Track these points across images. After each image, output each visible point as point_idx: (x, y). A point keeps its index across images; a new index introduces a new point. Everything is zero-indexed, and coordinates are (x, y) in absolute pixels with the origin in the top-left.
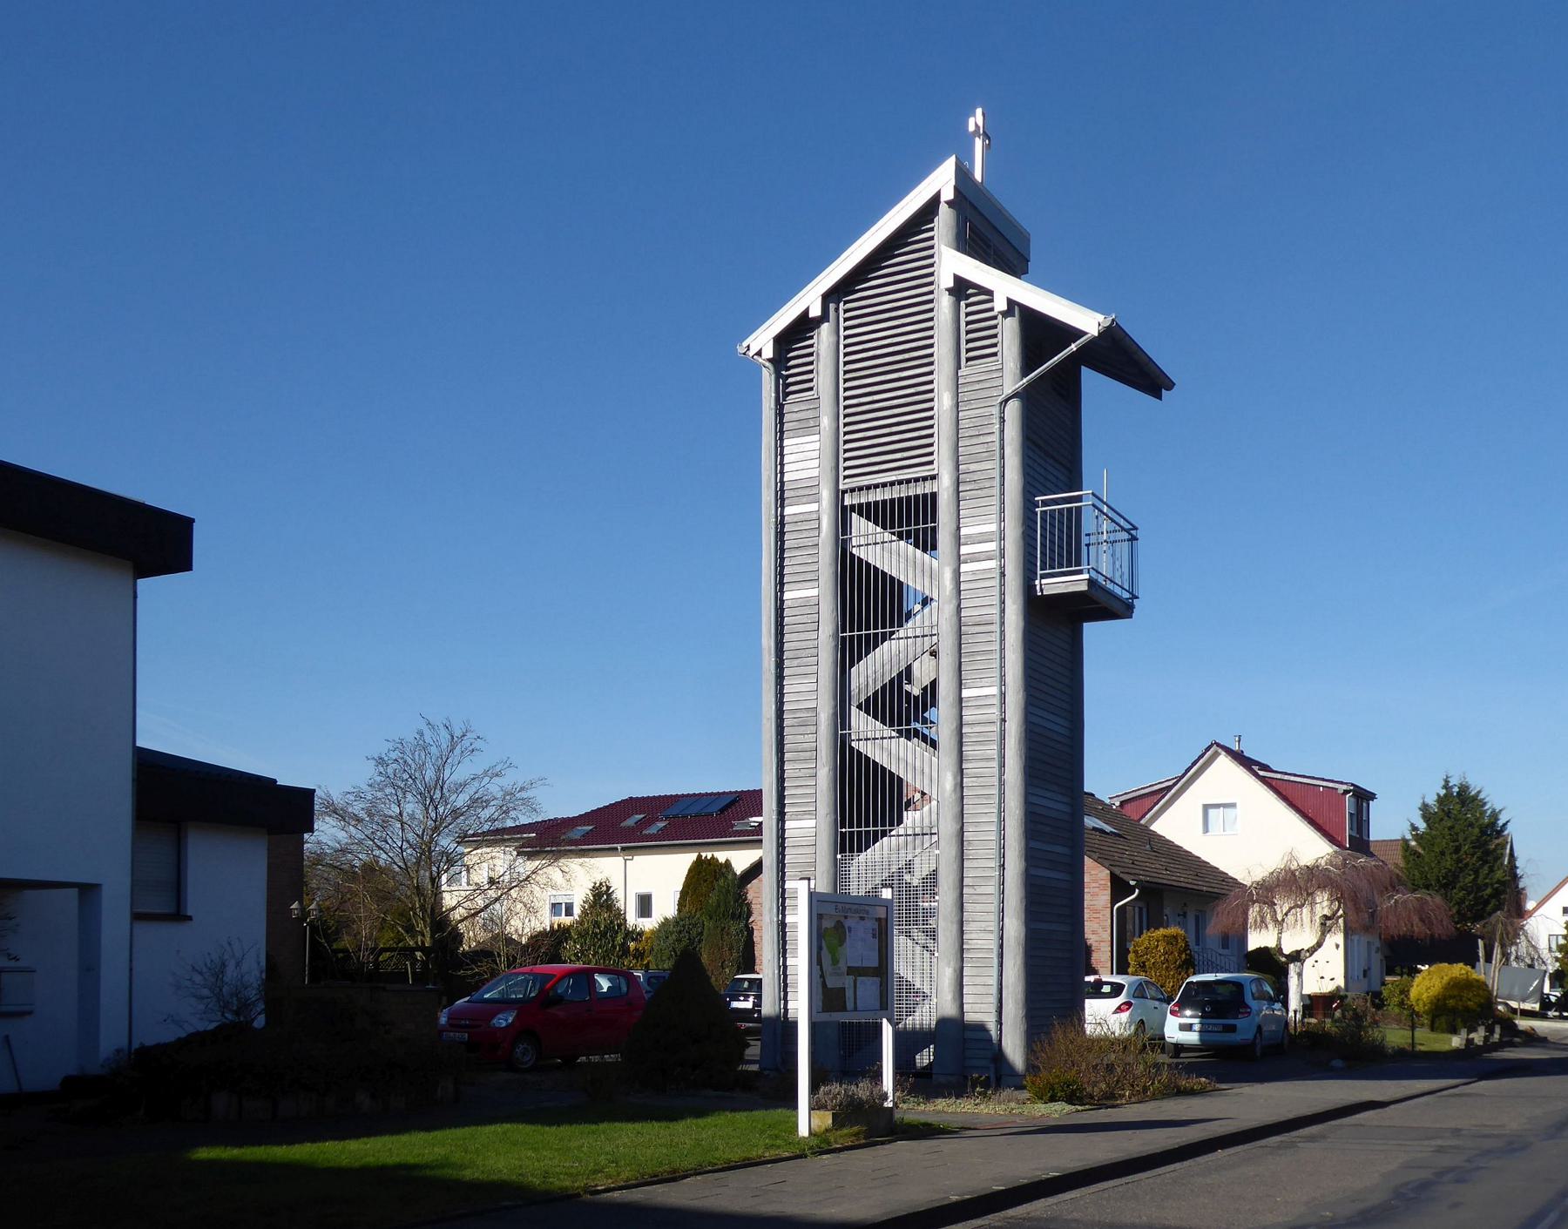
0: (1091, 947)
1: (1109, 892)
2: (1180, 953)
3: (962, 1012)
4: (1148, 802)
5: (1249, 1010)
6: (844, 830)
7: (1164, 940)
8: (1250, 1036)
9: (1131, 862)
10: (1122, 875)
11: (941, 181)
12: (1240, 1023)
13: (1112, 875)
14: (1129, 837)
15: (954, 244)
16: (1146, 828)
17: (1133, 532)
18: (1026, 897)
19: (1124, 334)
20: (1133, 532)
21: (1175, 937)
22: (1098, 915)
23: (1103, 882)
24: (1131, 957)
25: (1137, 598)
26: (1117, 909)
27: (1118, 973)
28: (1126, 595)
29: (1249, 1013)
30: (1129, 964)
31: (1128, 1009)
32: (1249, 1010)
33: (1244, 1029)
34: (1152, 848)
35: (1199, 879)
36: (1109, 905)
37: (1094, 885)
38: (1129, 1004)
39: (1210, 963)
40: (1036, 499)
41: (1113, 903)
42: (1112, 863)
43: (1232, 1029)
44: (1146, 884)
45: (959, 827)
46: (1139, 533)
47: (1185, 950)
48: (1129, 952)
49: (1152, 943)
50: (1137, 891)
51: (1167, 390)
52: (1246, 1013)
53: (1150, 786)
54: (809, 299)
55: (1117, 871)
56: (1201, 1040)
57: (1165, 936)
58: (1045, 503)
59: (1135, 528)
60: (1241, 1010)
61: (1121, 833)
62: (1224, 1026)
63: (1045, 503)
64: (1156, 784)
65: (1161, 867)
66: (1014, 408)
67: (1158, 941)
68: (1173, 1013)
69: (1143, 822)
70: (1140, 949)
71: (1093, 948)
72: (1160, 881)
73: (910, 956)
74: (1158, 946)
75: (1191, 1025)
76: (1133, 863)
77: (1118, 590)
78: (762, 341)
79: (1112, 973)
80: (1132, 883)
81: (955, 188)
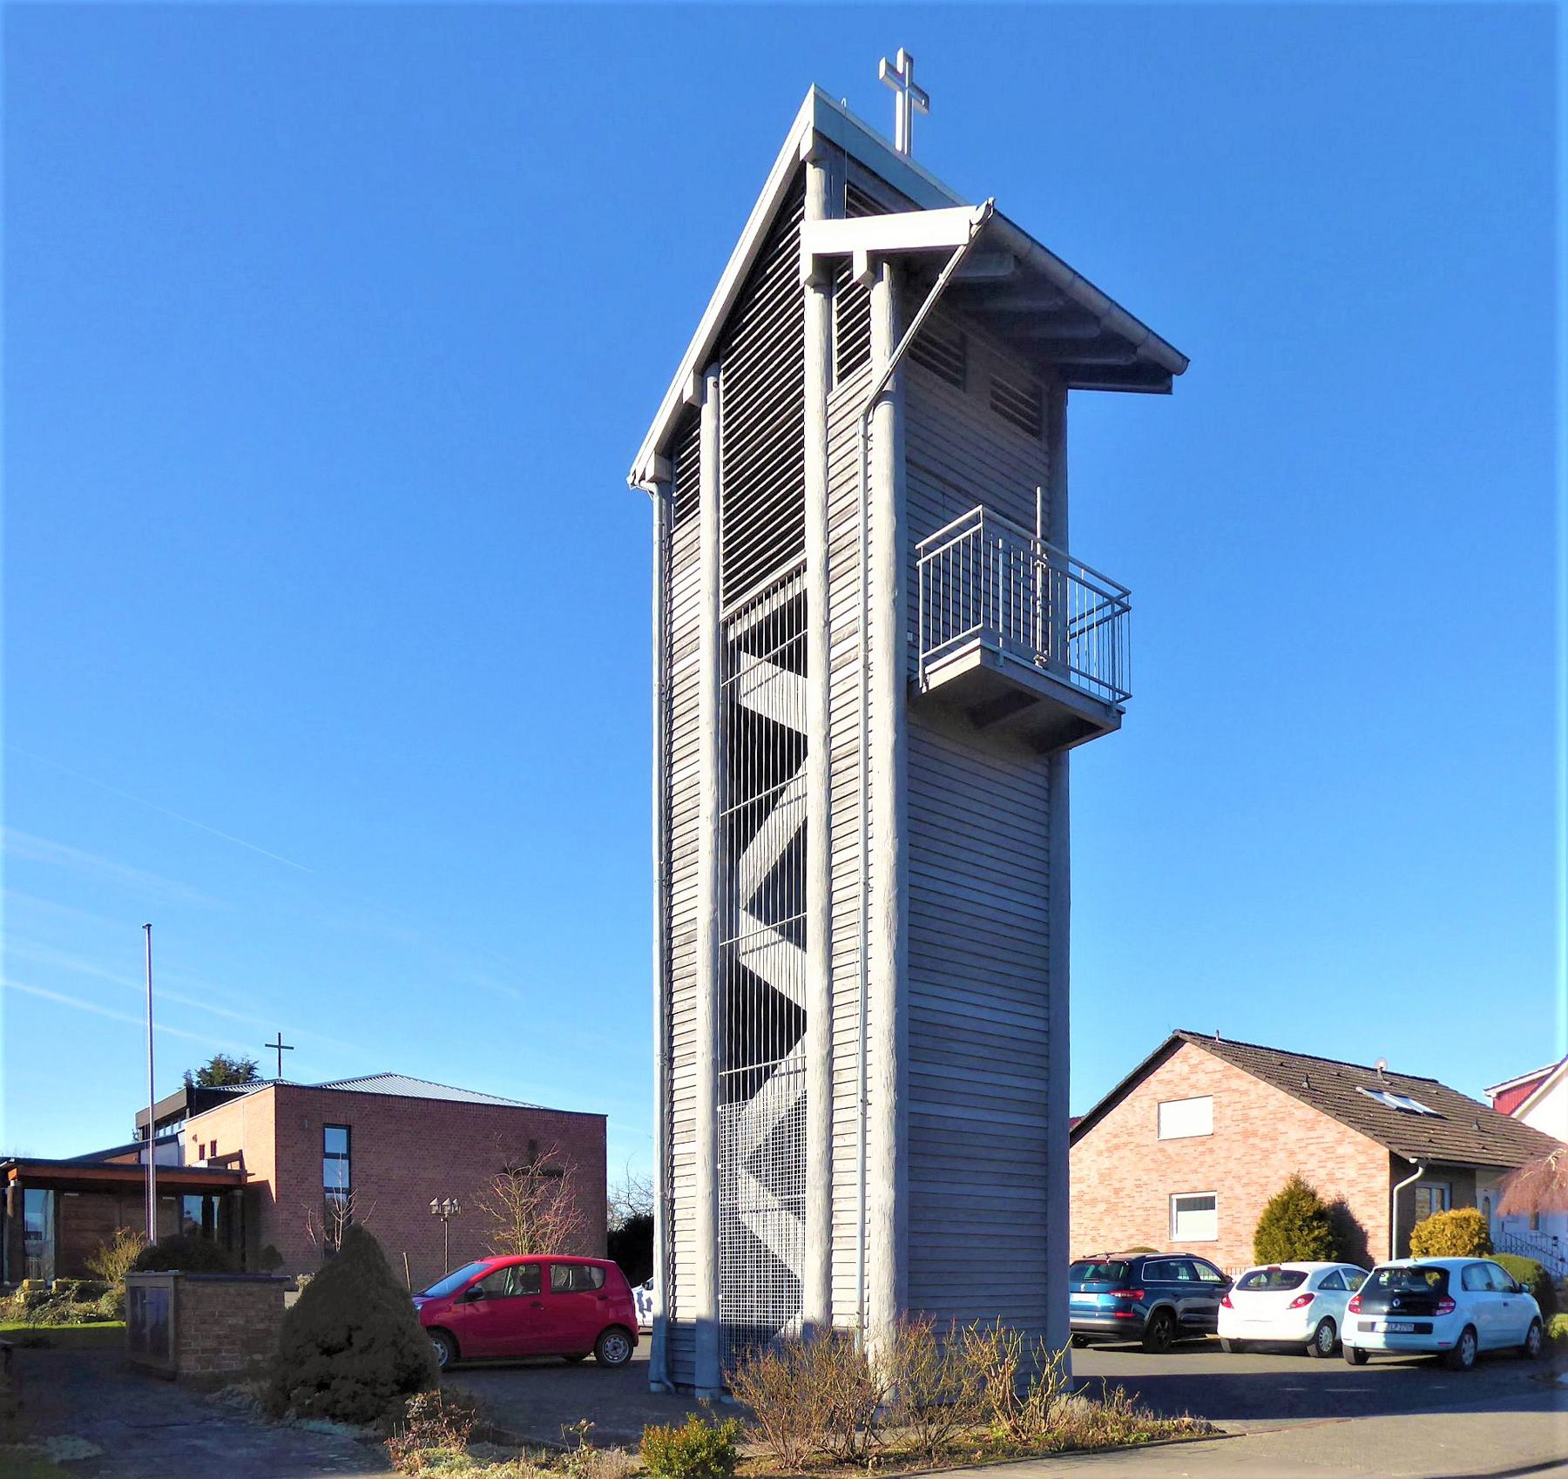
0: (1367, 1233)
1: (1389, 1171)
2: (1471, 1237)
3: (829, 1315)
4: (1527, 1090)
5: (1452, 1304)
6: (723, 1073)
7: (1452, 1223)
8: (1451, 1338)
9: (1428, 1139)
10: (1401, 1154)
11: (801, 136)
12: (1437, 1321)
13: (1392, 1154)
14: (1450, 1118)
15: (824, 216)
16: (1517, 1123)
17: (1124, 600)
18: (897, 1145)
19: (1028, 244)
20: (1124, 600)
21: (1467, 1220)
22: (1374, 1199)
23: (1381, 1162)
24: (1413, 1244)
25: (1128, 696)
26: (1400, 1191)
27: (1398, 1258)
28: (1105, 694)
29: (1453, 1308)
30: (1412, 1251)
31: (1306, 1303)
32: (1452, 1304)
33: (1445, 1329)
34: (1479, 1128)
35: (1433, 1145)
36: (1388, 1187)
37: (1372, 1166)
38: (1308, 1298)
39: (1529, 1248)
40: (917, 547)
41: (1393, 1184)
42: (1389, 1140)
43: (1426, 1329)
44: (1432, 1162)
45: (825, 1052)
46: (1131, 601)
47: (1478, 1234)
48: (1411, 1238)
49: (1437, 1227)
50: (1421, 1170)
51: (1178, 375)
52: (1448, 1308)
53: (1520, 1078)
54: (683, 384)
55: (1396, 1150)
56: (1386, 1343)
57: (1453, 1218)
58: (928, 550)
59: (1126, 593)
60: (1440, 1305)
61: (1440, 1113)
62: (1416, 1325)
63: (928, 550)
64: (1525, 1076)
65: (1477, 1146)
66: (884, 412)
67: (1444, 1224)
68: (1352, 1308)
69: (1514, 1115)
70: (1424, 1234)
71: (1369, 1234)
72: (1466, 1159)
73: (799, 1246)
74: (1444, 1230)
75: (1373, 1324)
76: (1430, 1141)
77: (1094, 689)
78: (645, 461)
79: (1391, 1259)
80: (1413, 1161)
81: (815, 130)
